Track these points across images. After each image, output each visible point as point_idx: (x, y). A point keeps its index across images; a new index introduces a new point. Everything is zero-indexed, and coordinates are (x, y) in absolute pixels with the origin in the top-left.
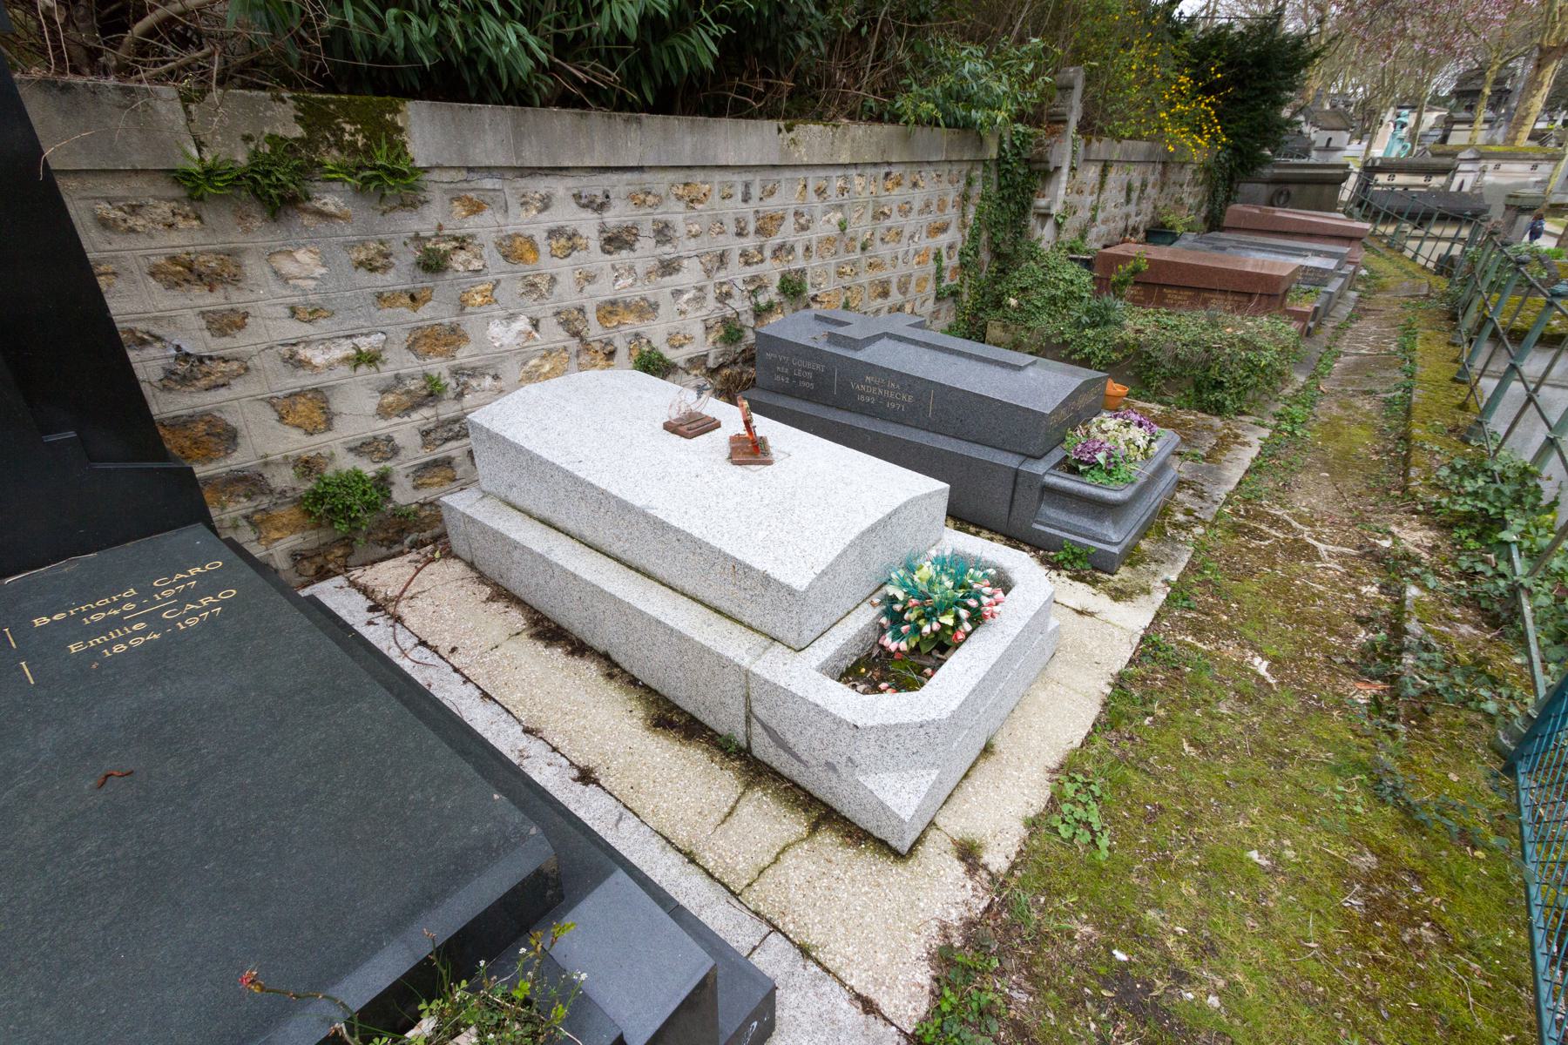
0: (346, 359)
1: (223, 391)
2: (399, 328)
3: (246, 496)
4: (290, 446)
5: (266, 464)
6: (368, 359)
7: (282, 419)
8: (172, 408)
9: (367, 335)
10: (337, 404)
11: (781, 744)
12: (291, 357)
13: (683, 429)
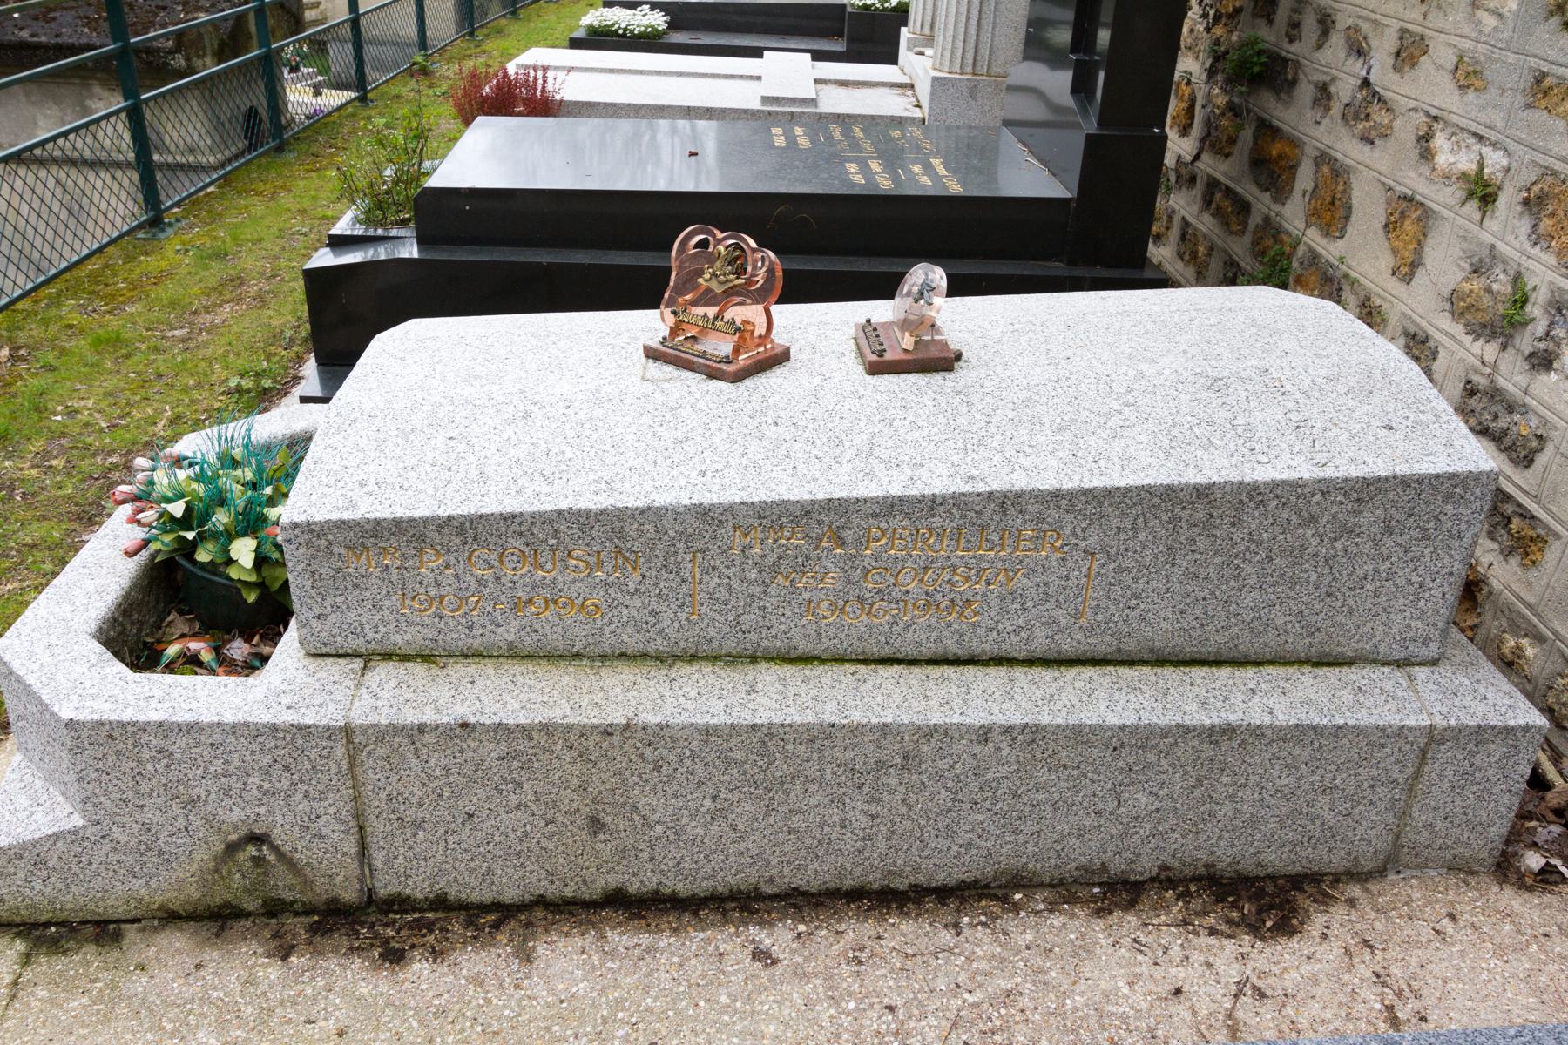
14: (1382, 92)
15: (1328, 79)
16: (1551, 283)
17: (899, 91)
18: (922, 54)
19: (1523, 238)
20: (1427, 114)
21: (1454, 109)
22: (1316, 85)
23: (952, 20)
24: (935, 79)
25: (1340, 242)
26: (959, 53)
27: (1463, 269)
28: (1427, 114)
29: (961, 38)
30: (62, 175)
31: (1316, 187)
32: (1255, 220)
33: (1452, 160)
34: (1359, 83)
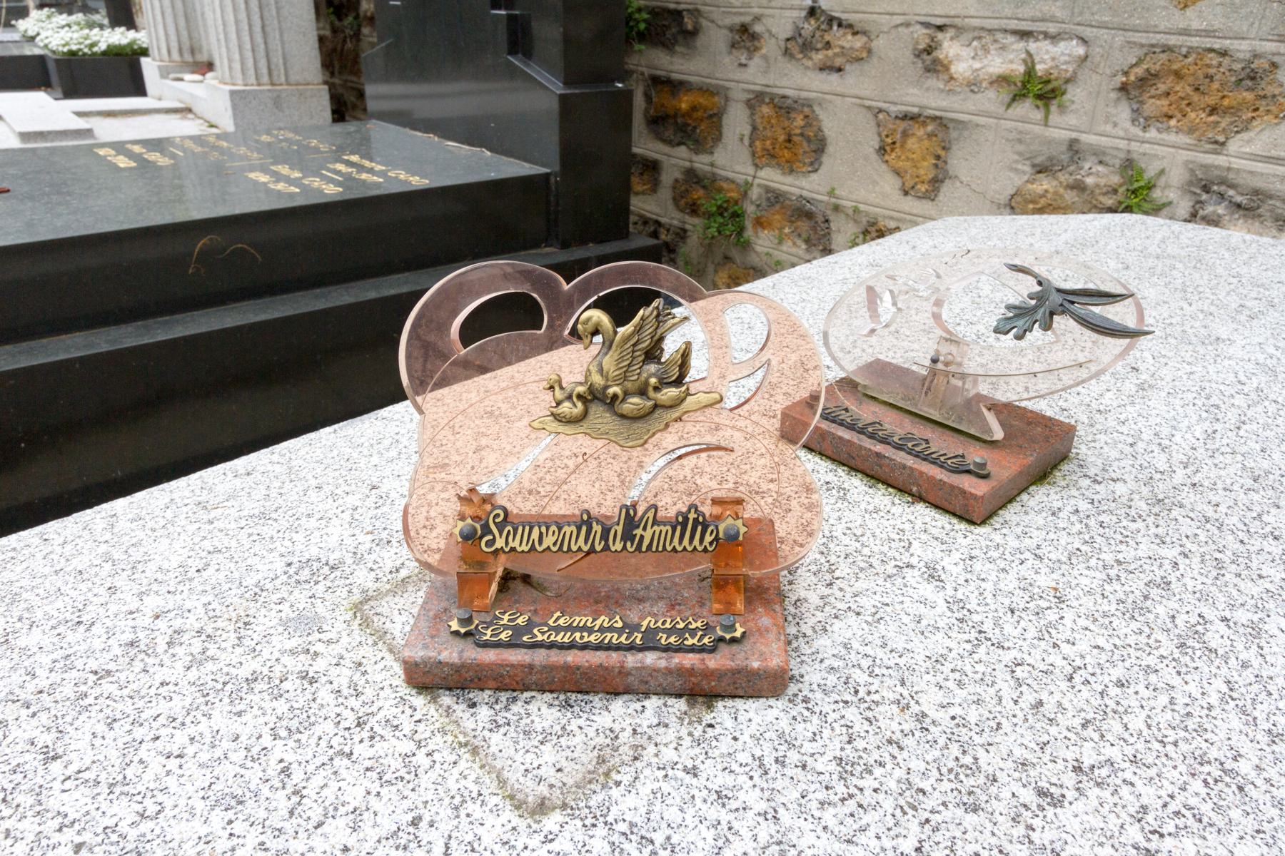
0: (1002, 80)
1: (834, 77)
2: (1119, 39)
3: (807, 241)
4: (872, 198)
5: (837, 208)
6: (1040, 90)
7: (882, 150)
8: (784, 82)
9: (1054, 38)
10: (958, 163)
11: (896, 104)
12: (929, 50)
13: (752, 272)
14: (843, 16)
15: (747, 19)
16: (1187, 163)
17: (178, 116)
18: (181, 80)
19: (1128, 124)
20: (926, 25)
21: (972, 12)
22: (731, 29)
23: (232, 29)
24: (232, 93)
25: (814, 176)
26: (250, 63)
27: (1024, 173)
28: (926, 25)
29: (248, 46)
30: (1153, 92)
31: (754, 128)
32: (668, 177)
33: (977, 65)
34: (803, 14)
